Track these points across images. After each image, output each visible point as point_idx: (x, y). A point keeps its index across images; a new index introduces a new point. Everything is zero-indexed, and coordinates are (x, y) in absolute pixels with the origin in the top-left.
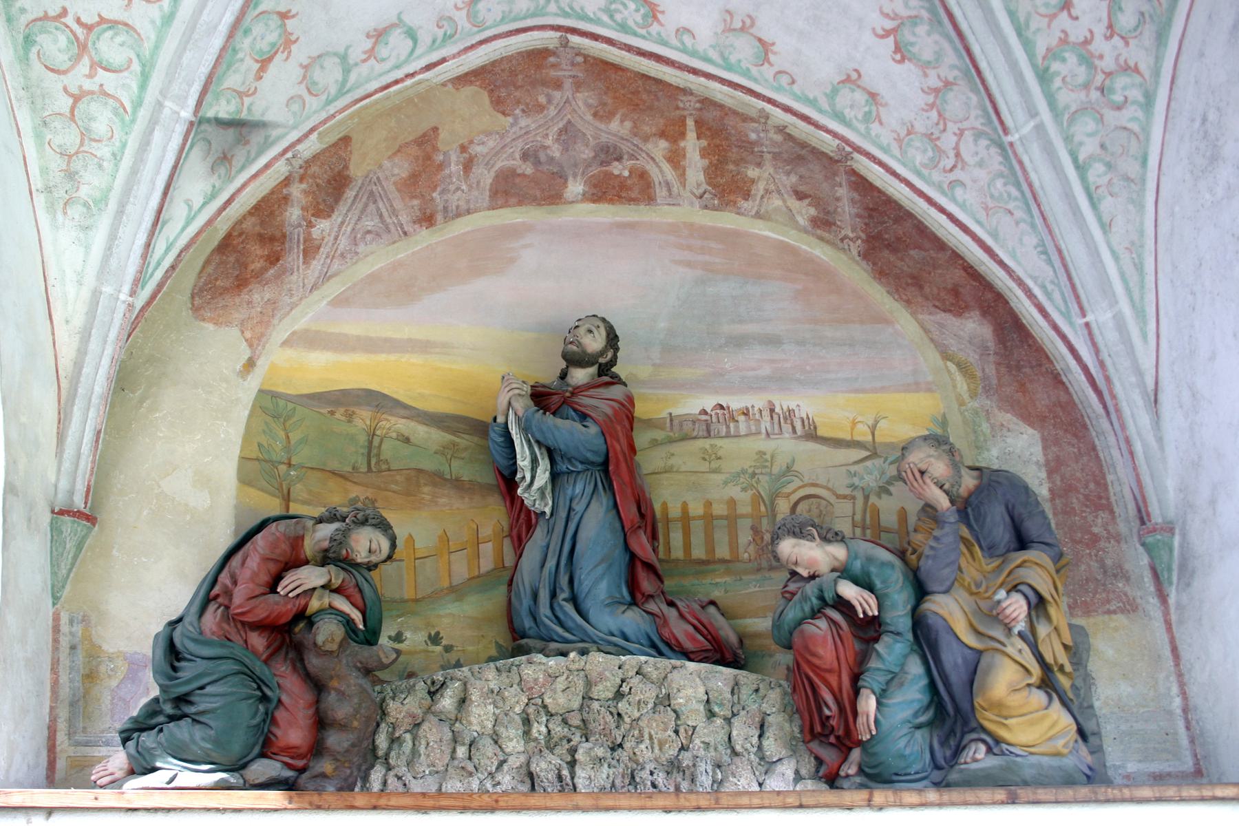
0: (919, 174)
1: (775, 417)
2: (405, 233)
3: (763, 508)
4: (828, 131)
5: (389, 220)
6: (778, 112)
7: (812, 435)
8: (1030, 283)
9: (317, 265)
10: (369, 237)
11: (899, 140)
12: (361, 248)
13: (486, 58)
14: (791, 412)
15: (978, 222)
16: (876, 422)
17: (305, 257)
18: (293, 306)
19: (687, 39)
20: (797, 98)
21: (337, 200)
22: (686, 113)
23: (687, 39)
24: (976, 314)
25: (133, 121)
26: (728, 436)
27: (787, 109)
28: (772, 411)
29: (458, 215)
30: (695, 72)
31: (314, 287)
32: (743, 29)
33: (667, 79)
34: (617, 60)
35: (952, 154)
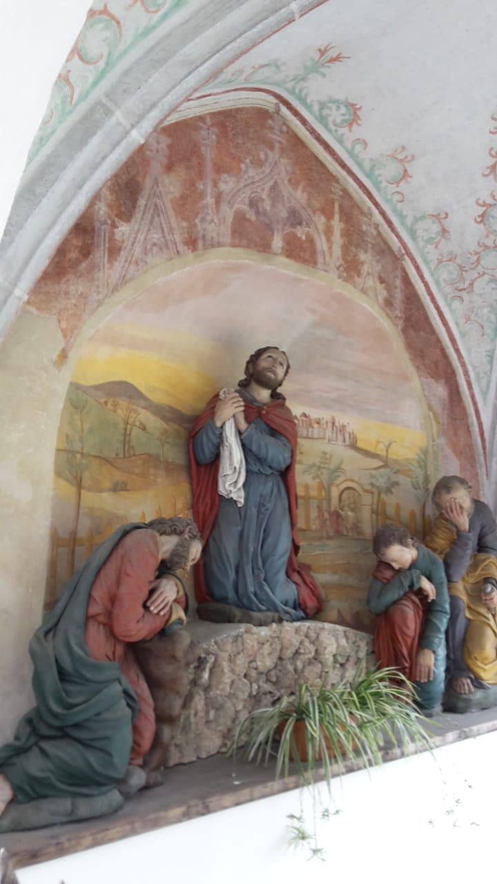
0: (437, 283)
1: (335, 428)
2: (178, 252)
3: (324, 494)
4: (398, 236)
5: (168, 237)
6: (378, 218)
7: (354, 446)
8: (470, 368)
9: (118, 265)
10: (155, 249)
11: (440, 261)
12: (149, 259)
13: (232, 103)
14: (344, 426)
15: (457, 324)
16: (390, 444)
17: (110, 257)
18: (100, 303)
19: (359, 148)
20: (394, 211)
21: (134, 207)
22: (335, 197)
23: (359, 148)
24: (443, 381)
25: (71, 112)
26: (307, 437)
27: (383, 213)
28: (333, 424)
29: (213, 246)
30: (344, 166)
31: (115, 289)
32: (401, 161)
33: (327, 164)
34: (303, 138)
35: (467, 283)
